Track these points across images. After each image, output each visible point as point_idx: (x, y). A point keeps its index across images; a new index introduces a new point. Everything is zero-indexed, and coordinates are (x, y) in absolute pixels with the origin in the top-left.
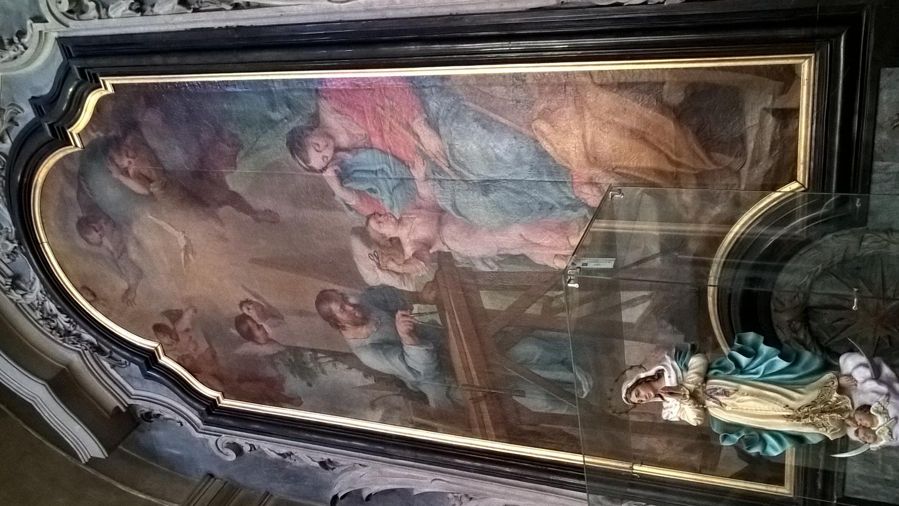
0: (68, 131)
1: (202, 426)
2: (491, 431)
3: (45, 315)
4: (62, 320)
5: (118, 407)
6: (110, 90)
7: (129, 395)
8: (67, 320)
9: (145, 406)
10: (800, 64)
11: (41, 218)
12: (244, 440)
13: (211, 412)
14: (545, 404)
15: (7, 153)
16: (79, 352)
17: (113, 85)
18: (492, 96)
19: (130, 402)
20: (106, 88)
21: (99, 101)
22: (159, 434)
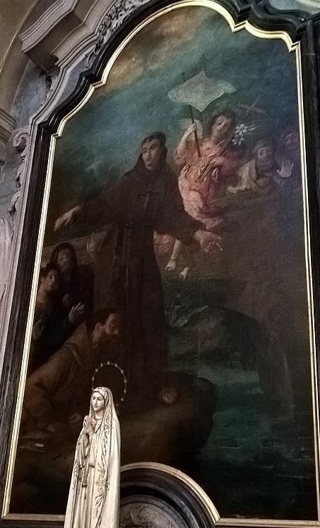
0: (247, 21)
1: (38, 122)
2: (35, 378)
3: (118, 10)
4: (116, 23)
5: (58, 59)
6: (291, 49)
7: (67, 66)
8: (119, 25)
9: (55, 81)
10: (317, 520)
11: (162, 15)
12: (29, 153)
13: (47, 130)
14: (72, 243)
15: (55, 54)
16: (94, 33)
17: (295, 51)
18: (145, 126)
19: (62, 67)
20: (292, 46)
21: (284, 41)
22: (40, 84)
